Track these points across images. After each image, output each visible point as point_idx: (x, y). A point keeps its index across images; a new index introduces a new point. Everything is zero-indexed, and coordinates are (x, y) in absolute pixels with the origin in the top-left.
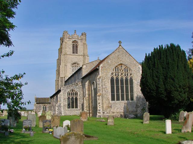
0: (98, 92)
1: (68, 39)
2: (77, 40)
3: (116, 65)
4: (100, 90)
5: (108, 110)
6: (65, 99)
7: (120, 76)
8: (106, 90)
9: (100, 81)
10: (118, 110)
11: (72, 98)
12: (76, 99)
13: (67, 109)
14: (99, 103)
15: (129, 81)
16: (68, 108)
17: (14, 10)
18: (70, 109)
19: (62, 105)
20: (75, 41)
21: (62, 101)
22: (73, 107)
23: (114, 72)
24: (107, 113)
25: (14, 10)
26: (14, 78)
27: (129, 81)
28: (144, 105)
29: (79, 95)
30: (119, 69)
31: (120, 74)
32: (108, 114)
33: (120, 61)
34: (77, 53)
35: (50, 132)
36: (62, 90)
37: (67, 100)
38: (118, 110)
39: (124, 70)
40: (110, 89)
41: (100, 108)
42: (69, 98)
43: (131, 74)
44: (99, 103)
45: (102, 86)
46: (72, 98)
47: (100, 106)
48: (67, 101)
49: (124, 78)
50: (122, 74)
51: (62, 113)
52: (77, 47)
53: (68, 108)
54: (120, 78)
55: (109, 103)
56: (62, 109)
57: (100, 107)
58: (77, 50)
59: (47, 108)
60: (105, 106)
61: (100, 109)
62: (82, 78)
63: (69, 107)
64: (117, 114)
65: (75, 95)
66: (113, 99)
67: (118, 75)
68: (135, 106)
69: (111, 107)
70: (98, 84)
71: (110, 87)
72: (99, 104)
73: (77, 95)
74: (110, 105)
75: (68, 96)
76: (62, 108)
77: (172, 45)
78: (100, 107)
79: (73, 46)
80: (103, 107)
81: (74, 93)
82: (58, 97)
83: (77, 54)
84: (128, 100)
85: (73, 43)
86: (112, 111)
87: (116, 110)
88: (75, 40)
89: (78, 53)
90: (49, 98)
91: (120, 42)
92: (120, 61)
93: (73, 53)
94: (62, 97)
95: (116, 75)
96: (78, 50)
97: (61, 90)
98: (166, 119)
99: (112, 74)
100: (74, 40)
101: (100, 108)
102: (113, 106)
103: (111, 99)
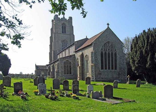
3: (105, 42)
4: (93, 62)
7: (107, 51)
8: (97, 61)
9: (94, 54)
10: (106, 76)
15: (104, 54)
17: (4, 54)
20: (64, 23)
25: (4, 54)
27: (104, 54)
29: (73, 64)
30: (107, 46)
31: (107, 50)
33: (108, 39)
35: (43, 92)
38: (106, 76)
39: (110, 47)
42: (65, 66)
43: (115, 50)
45: (95, 58)
49: (110, 53)
50: (109, 50)
52: (65, 28)
54: (107, 53)
60: (97, 73)
65: (70, 64)
66: (102, 68)
67: (106, 50)
68: (118, 74)
69: (101, 74)
77: (71, 17)
79: (63, 27)
80: (95, 74)
81: (69, 63)
84: (110, 69)
85: (62, 24)
86: (101, 76)
92: (108, 39)
93: (63, 32)
95: (105, 50)
99: (102, 49)
103: (101, 69)
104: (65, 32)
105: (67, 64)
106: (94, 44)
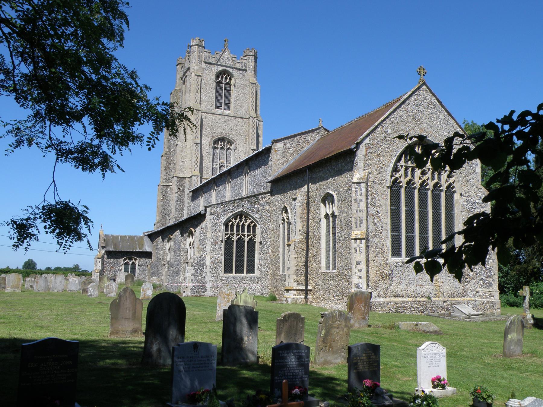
0: (354, 225)
1: (204, 65)
2: (230, 70)
5: (383, 285)
6: (216, 242)
11: (240, 241)
12: (252, 243)
13: (222, 274)
14: (358, 263)
16: (225, 272)
18: (242, 275)
19: (208, 261)
21: (208, 249)
22: (240, 270)
23: (402, 166)
24: (379, 296)
26: (118, 166)
28: (488, 277)
32: (382, 300)
34: (229, 109)
36: (208, 214)
37: (223, 245)
40: (389, 217)
41: (360, 277)
44: (358, 263)
46: (240, 241)
47: (360, 271)
48: (223, 249)
51: (208, 286)
53: (225, 272)
55: (386, 264)
56: (208, 274)
57: (359, 274)
58: (228, 97)
59: (137, 266)
61: (361, 280)
62: (270, 182)
63: (228, 269)
64: (408, 299)
69: (390, 276)
70: (356, 201)
71: (389, 211)
72: (359, 267)
73: (254, 231)
74: (387, 270)
75: (226, 235)
76: (208, 270)
78: (359, 274)
81: (247, 224)
82: (336, 222)
83: (228, 112)
87: (403, 286)
88: (224, 68)
89: (232, 106)
90: (141, 238)
91: (421, 72)
94: (209, 236)
96: (232, 101)
97: (205, 214)
98: (238, 338)
99: (395, 170)
100: (220, 68)
101: (360, 277)
102: (395, 274)
103: (390, 255)
104: (227, 105)
105: (238, 230)
106: (367, 150)
